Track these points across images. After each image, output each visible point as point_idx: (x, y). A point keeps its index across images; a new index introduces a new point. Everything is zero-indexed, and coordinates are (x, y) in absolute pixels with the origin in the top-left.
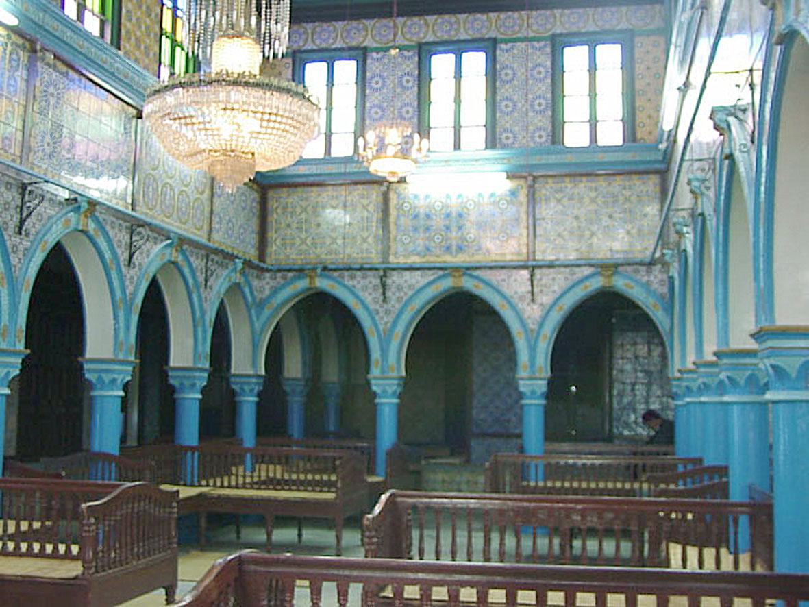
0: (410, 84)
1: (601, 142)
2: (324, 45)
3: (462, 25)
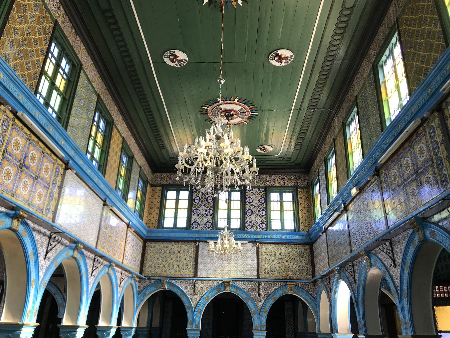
1: (178, 226)
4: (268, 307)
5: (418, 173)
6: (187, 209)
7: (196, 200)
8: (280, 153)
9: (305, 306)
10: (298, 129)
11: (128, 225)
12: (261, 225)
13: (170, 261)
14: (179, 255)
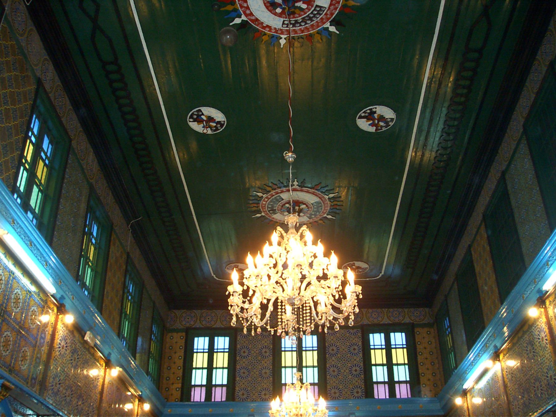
0: (267, 354)
2: (208, 325)
8: (381, 275)
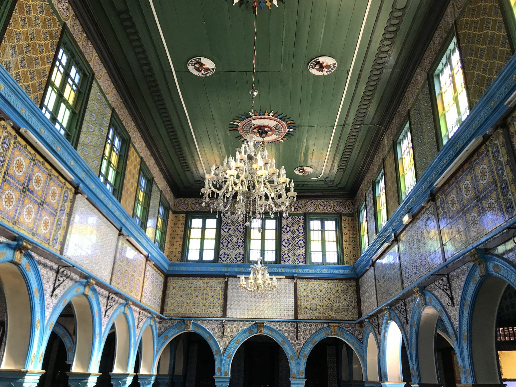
1: (204, 258)
3: (347, 208)
4: (307, 351)
5: (480, 198)
6: (215, 239)
7: (225, 229)
8: (321, 176)
9: (350, 350)
10: (342, 148)
11: (147, 258)
12: (299, 258)
13: (195, 299)
14: (205, 291)
